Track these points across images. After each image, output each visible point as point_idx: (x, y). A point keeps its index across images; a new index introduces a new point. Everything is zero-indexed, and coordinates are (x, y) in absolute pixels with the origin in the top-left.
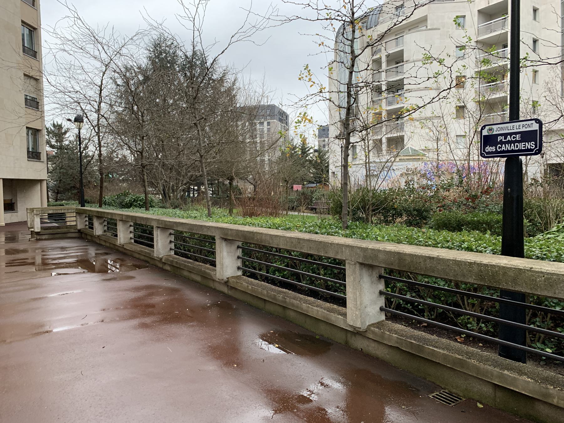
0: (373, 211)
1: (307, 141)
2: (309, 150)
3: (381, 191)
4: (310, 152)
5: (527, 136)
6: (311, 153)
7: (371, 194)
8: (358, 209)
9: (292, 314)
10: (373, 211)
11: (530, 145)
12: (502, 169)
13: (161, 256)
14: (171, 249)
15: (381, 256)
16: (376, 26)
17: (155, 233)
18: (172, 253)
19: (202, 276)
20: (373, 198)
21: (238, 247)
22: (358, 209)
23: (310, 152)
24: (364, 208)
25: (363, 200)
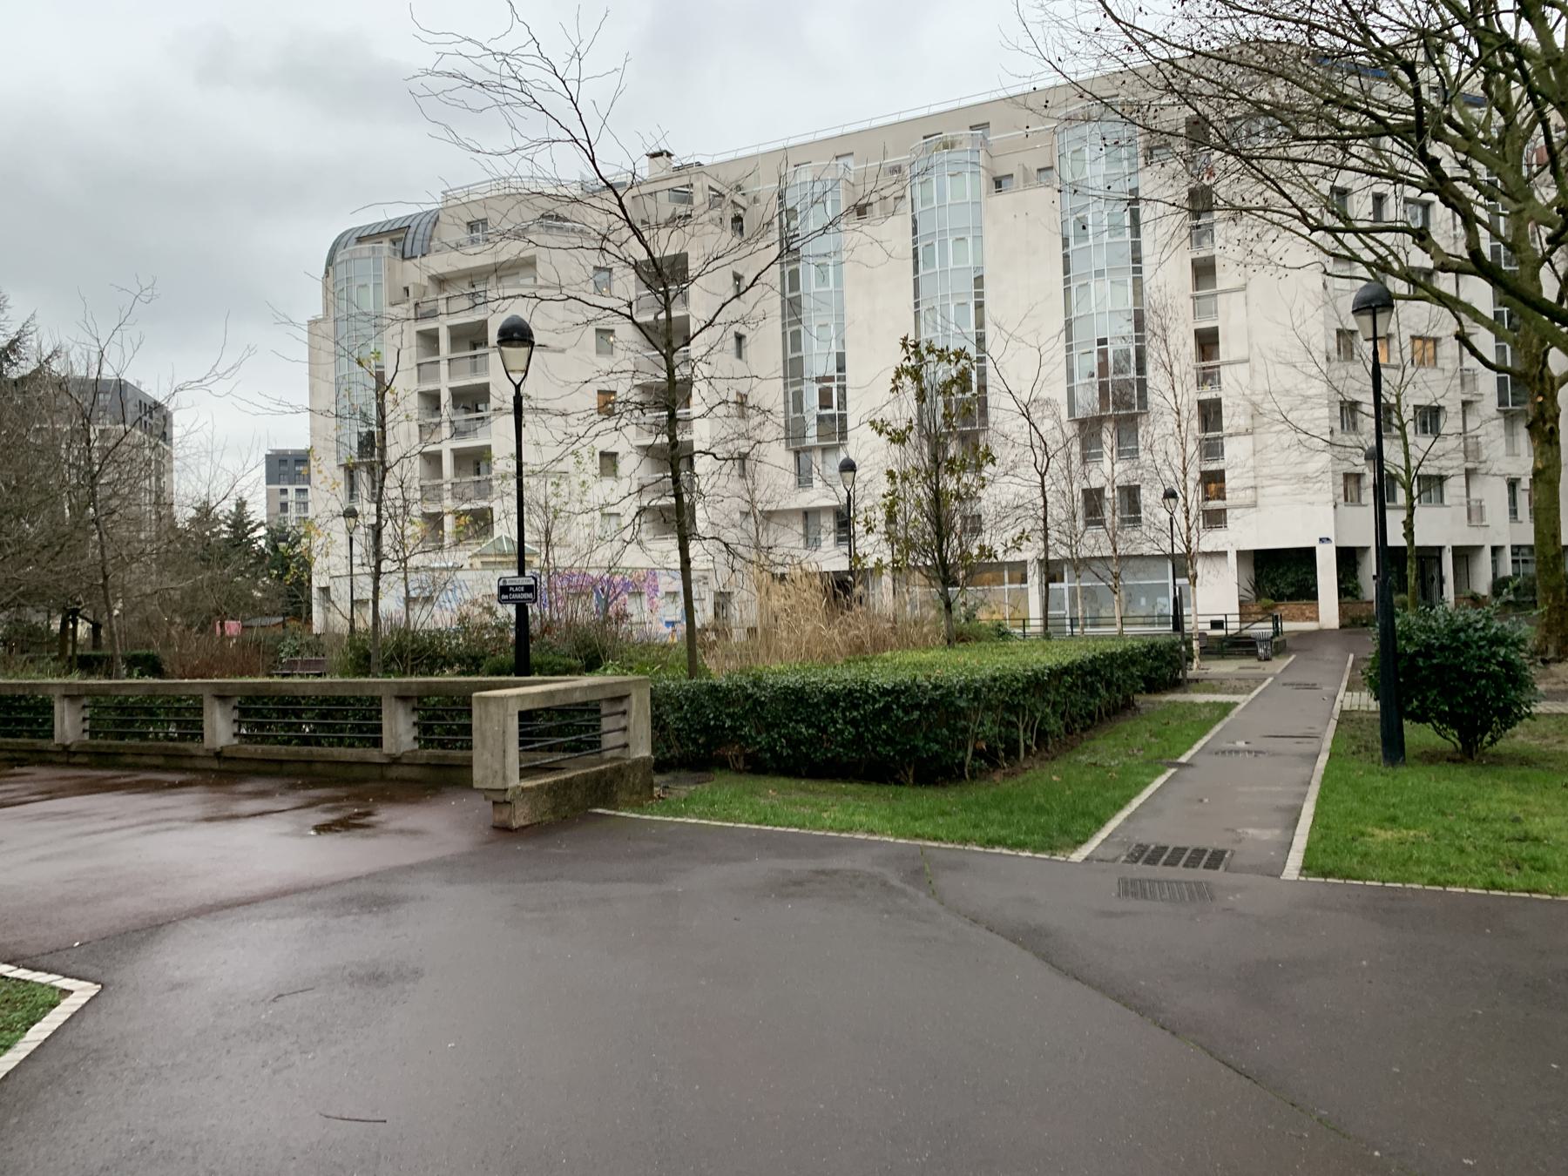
0: (413, 660)
1: (249, 508)
2: (254, 530)
3: (424, 631)
4: (256, 534)
5: (529, 589)
6: (260, 537)
7: (410, 637)
8: (392, 659)
9: (319, 767)
10: (413, 660)
11: (530, 596)
12: (513, 614)
13: (68, 743)
14: (84, 731)
15: (414, 687)
16: (424, 255)
17: (57, 706)
18: (86, 736)
19: (165, 756)
20: (413, 641)
21: (235, 708)
22: (392, 659)
23: (256, 534)
24: (400, 657)
25: (398, 645)
